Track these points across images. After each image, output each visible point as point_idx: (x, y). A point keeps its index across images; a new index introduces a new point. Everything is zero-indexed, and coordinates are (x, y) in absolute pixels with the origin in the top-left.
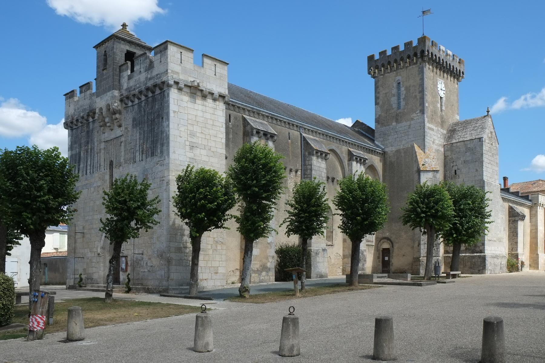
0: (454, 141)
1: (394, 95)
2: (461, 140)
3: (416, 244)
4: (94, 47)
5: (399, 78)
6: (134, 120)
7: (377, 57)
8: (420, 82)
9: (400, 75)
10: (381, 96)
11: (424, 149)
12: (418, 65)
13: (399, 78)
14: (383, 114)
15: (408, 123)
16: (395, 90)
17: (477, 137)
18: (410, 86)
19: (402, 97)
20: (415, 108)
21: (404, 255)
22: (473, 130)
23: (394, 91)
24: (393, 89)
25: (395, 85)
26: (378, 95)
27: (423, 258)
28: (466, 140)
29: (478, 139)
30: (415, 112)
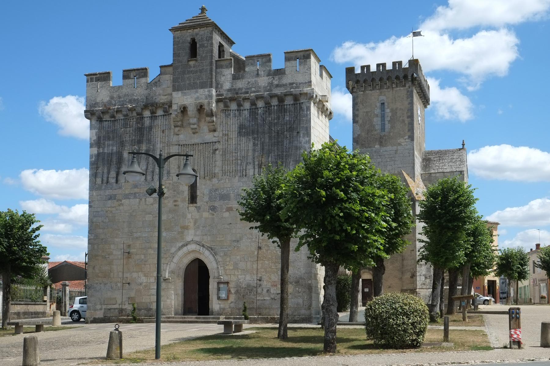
0: (433, 171)
1: (377, 116)
2: (441, 170)
3: (408, 275)
4: (284, 53)
5: (382, 98)
6: (241, 127)
7: (358, 71)
8: (409, 106)
9: (385, 95)
10: (361, 113)
11: (414, 177)
12: (406, 88)
13: (382, 98)
14: (363, 134)
15: (395, 148)
16: (378, 110)
17: (458, 170)
18: (396, 109)
19: (387, 119)
20: (402, 133)
21: (389, 287)
22: (451, 162)
23: (378, 111)
24: (376, 108)
25: (378, 105)
26: (357, 113)
27: (420, 290)
28: (446, 171)
29: (459, 172)
30: (403, 137)
